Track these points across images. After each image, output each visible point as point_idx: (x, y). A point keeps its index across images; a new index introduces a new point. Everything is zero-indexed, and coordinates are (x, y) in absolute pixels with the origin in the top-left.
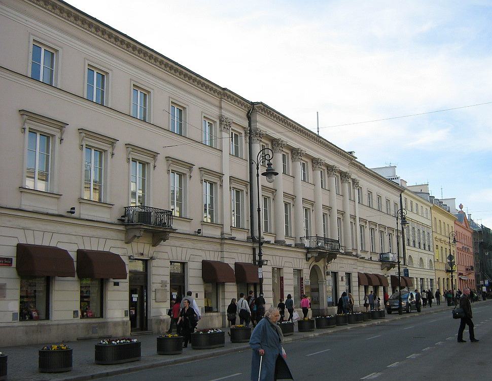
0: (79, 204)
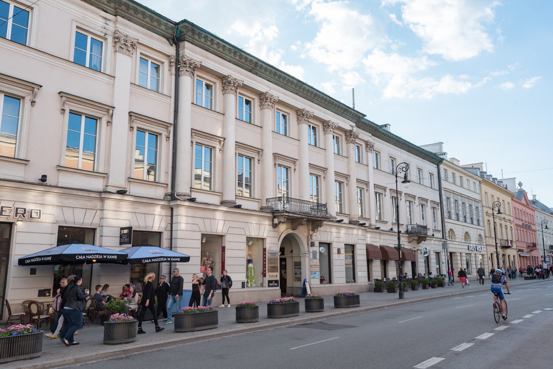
0: (57, 171)
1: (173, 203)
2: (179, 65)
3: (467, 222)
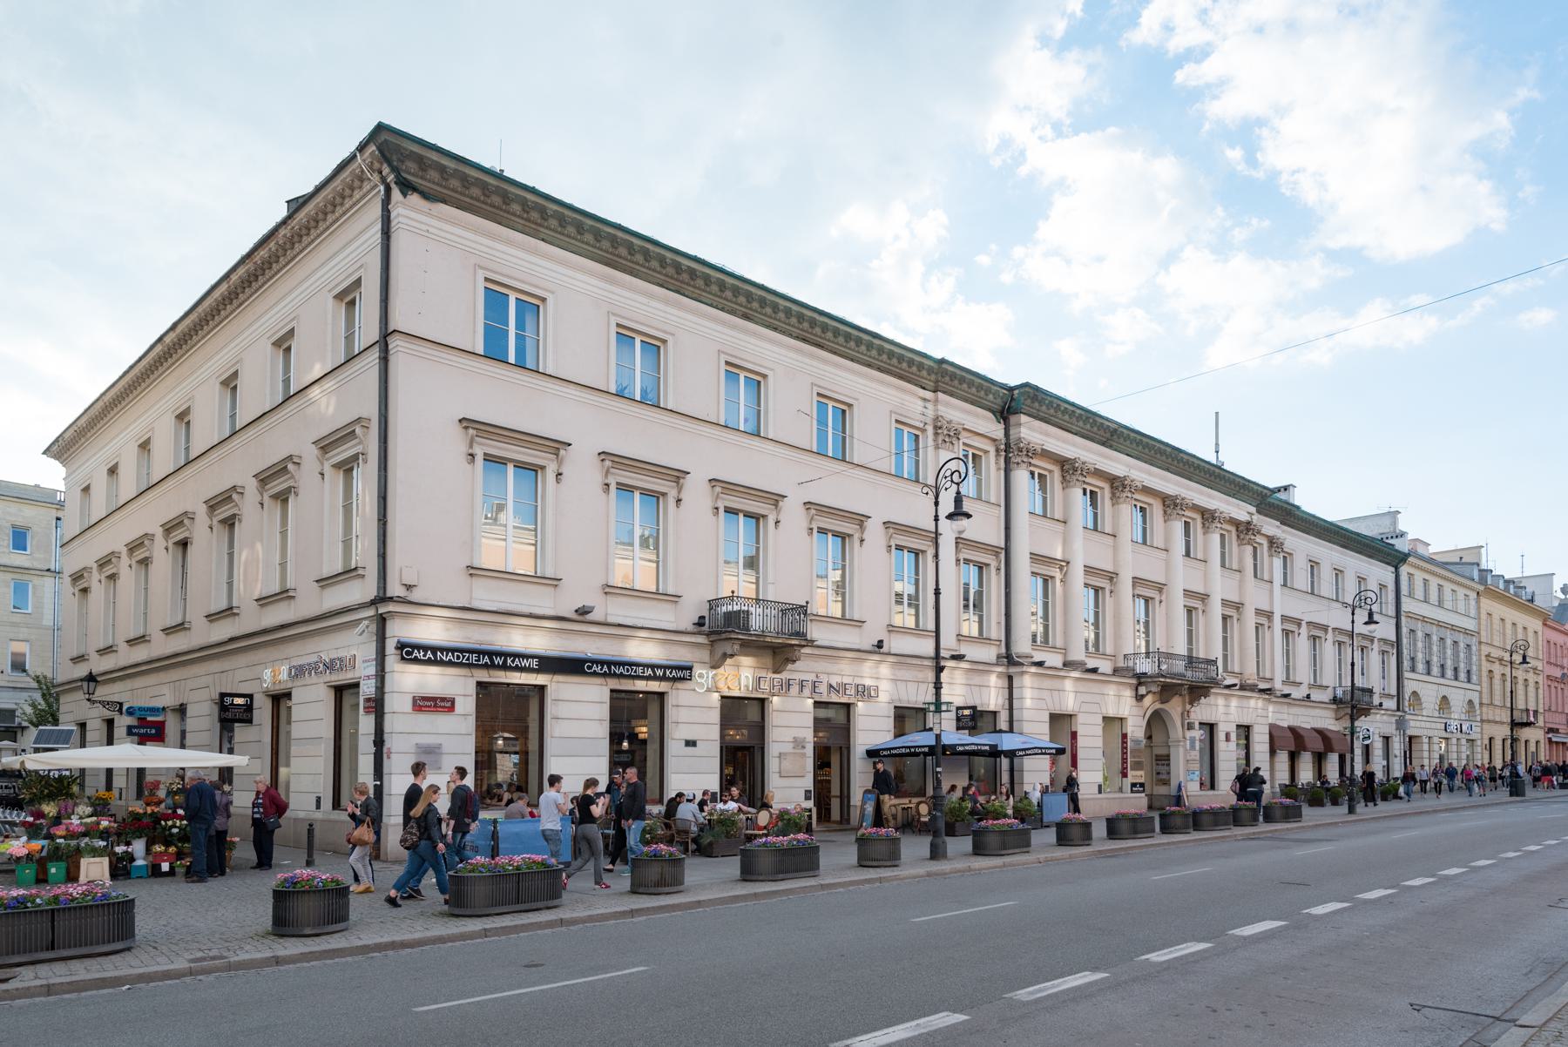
0: (469, 577)
1: (1013, 670)
2: (1010, 452)
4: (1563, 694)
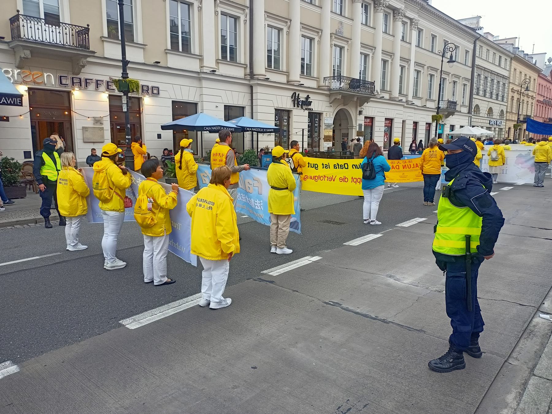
3: (504, 101)
4: (551, 111)
